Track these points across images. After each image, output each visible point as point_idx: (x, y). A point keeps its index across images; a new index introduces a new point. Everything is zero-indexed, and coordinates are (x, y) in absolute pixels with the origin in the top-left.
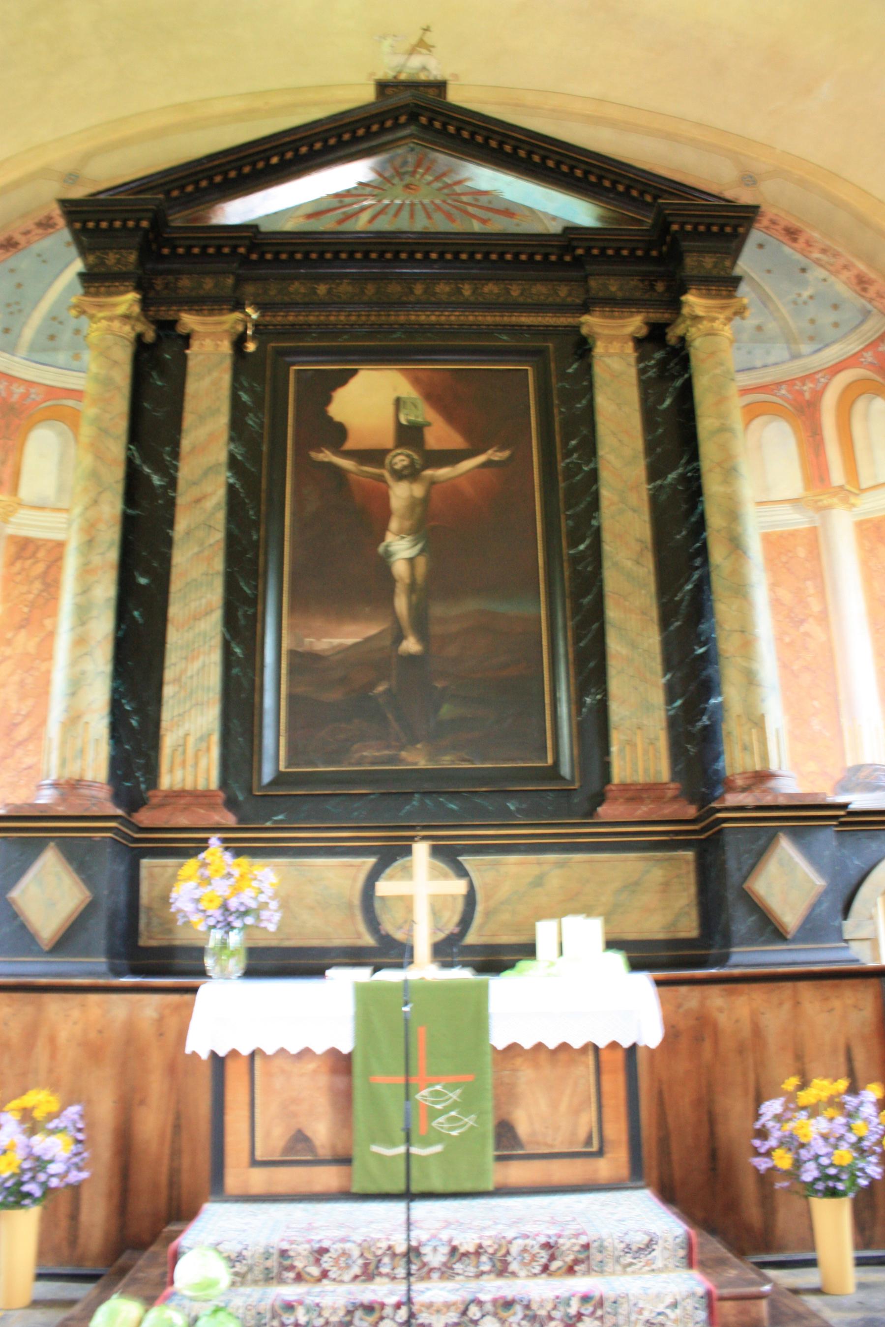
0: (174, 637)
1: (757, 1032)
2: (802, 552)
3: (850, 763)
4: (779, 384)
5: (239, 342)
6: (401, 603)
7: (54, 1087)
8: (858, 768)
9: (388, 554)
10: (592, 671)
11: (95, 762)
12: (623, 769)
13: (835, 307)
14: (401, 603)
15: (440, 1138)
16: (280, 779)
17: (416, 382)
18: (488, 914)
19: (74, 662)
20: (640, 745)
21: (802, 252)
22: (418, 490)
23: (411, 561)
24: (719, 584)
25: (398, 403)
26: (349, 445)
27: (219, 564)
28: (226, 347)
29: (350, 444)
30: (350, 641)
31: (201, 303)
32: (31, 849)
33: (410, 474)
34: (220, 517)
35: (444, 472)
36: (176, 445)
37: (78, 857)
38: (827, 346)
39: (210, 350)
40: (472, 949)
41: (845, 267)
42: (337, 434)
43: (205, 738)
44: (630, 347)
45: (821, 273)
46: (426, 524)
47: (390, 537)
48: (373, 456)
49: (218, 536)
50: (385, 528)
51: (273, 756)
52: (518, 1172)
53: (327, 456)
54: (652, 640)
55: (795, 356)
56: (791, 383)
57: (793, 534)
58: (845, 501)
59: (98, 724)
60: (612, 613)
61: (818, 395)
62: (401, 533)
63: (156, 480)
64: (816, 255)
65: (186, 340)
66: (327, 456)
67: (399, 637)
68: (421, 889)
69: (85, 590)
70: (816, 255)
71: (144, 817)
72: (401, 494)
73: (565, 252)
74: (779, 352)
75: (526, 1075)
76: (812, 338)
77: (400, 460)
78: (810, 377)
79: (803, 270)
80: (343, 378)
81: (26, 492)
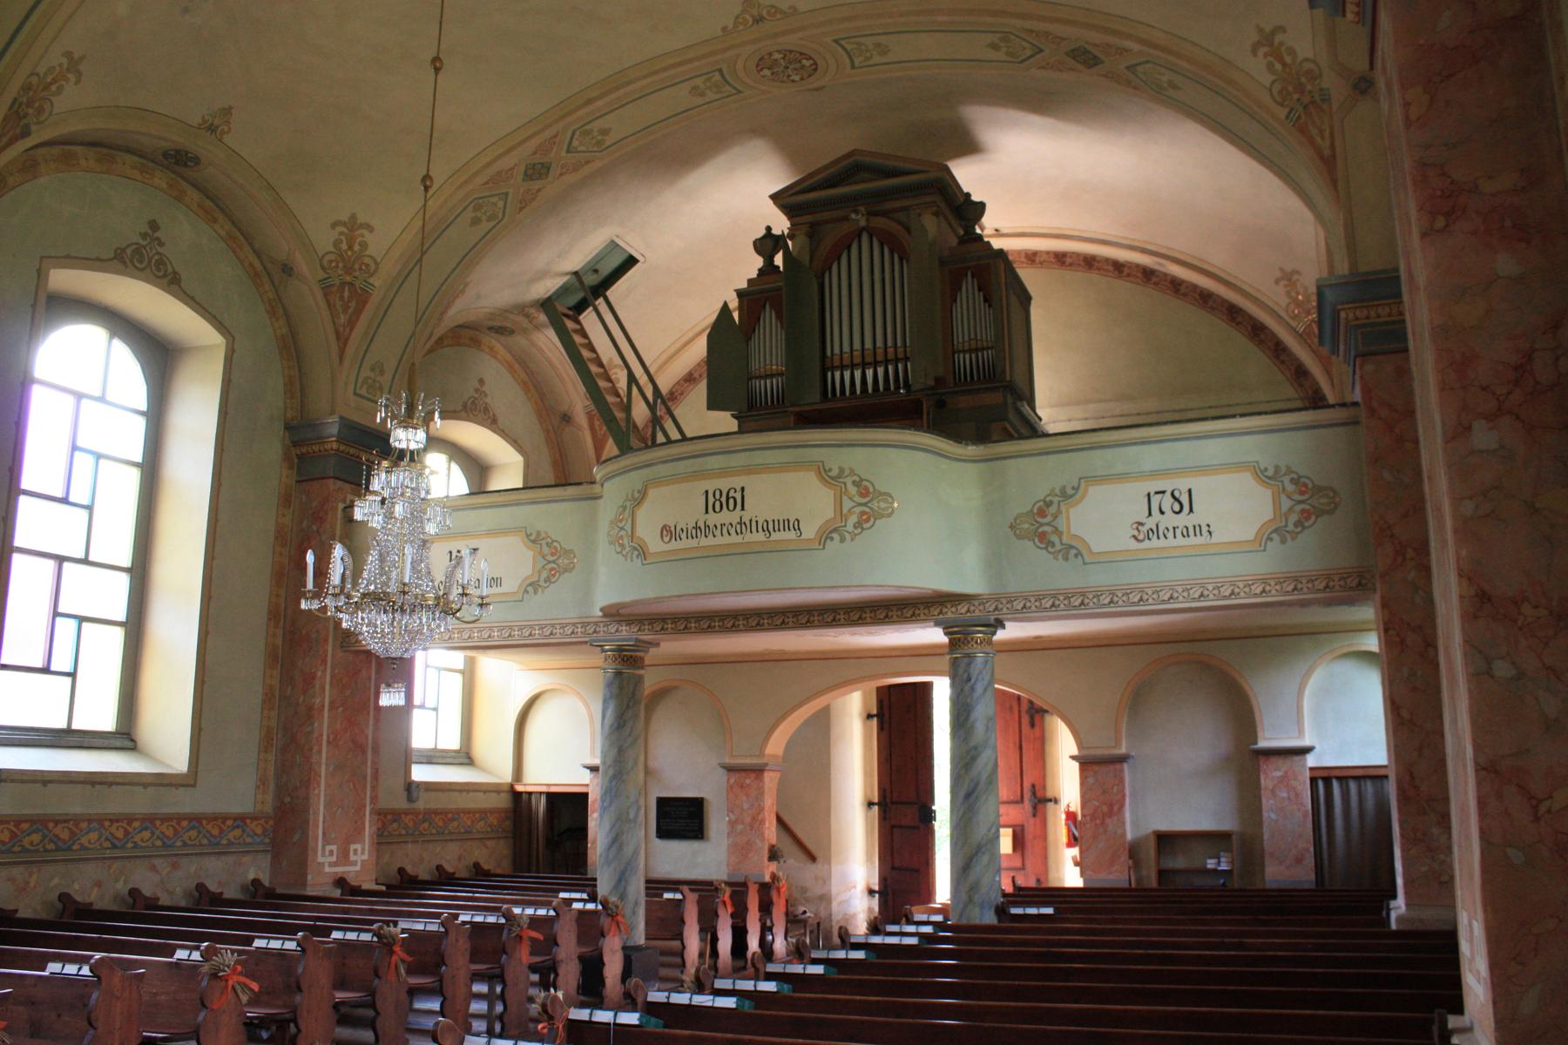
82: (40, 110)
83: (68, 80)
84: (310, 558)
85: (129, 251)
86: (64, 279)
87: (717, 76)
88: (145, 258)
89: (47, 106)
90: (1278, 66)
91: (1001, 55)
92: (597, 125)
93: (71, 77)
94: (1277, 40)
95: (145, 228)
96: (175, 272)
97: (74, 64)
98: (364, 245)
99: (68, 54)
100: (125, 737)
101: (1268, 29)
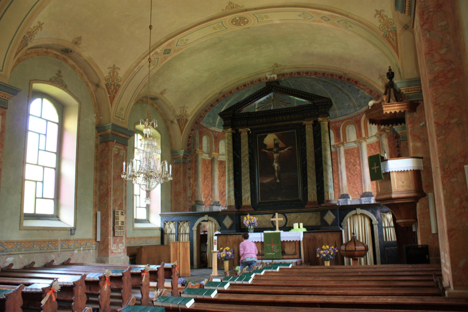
0: (243, 182)
1: (322, 239)
2: (356, 152)
3: (364, 192)
4: (352, 117)
5: (248, 132)
6: (276, 174)
7: (229, 247)
8: (365, 193)
9: (274, 166)
10: (305, 184)
11: (233, 203)
12: (310, 199)
13: (365, 98)
14: (276, 174)
15: (275, 252)
16: (260, 203)
17: (277, 135)
18: (289, 222)
19: (228, 188)
20: (312, 195)
21: (358, 87)
22: (278, 155)
23: (277, 167)
24: (324, 170)
25: (274, 140)
26: (267, 148)
27: (248, 170)
28: (246, 133)
29: (267, 148)
30: (269, 181)
31: (242, 126)
32: (225, 216)
33: (277, 152)
34: (248, 163)
35: (282, 151)
36: (241, 152)
37: (231, 217)
38: (363, 107)
39: (244, 133)
40: (287, 227)
41: (368, 89)
42: (265, 145)
43: (248, 198)
44: (311, 126)
45: (362, 91)
46: (280, 161)
47: (274, 163)
48: (271, 150)
49: (248, 166)
50: (273, 162)
51: (259, 199)
52: (285, 257)
53: (264, 150)
54: (315, 178)
55: (356, 111)
56: (355, 117)
57: (354, 148)
58: (365, 140)
59: (233, 197)
60: (308, 174)
61: (360, 118)
62: (276, 163)
63: (238, 157)
64: (361, 87)
65: (240, 133)
66: (264, 150)
67: (276, 180)
68: (278, 219)
69: (229, 177)
70: (361, 87)
71: (240, 210)
72: (275, 156)
73: (300, 109)
74: (353, 110)
75: (286, 245)
76: (360, 106)
77: (275, 150)
78: (359, 115)
79: (358, 91)
80: (265, 136)
81: (220, 152)
82: (31, 39)
83: (39, 30)
84: (124, 164)
85: (53, 79)
86: (38, 86)
87: (221, 24)
88: (57, 81)
89: (33, 37)
90: (382, 20)
91: (302, 18)
92: (184, 38)
93: (40, 29)
94: (382, 13)
95: (57, 73)
96: (65, 85)
97: (40, 25)
98: (118, 74)
99: (39, 22)
100: (56, 216)
101: (379, 10)
